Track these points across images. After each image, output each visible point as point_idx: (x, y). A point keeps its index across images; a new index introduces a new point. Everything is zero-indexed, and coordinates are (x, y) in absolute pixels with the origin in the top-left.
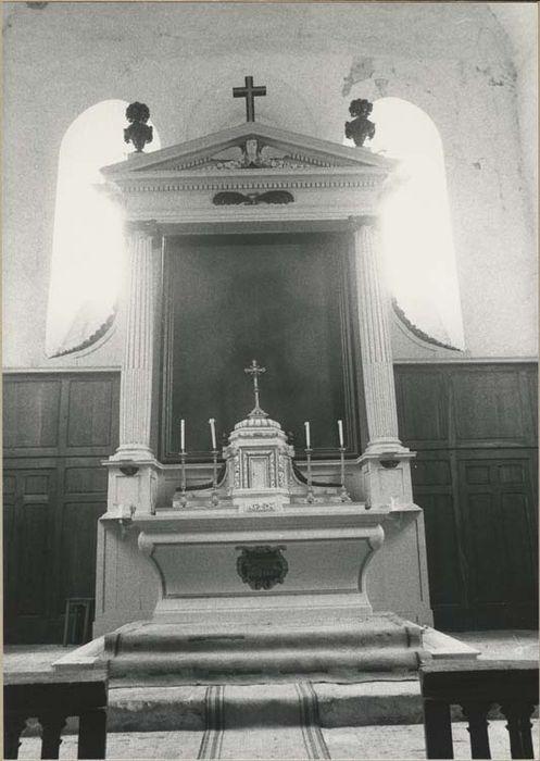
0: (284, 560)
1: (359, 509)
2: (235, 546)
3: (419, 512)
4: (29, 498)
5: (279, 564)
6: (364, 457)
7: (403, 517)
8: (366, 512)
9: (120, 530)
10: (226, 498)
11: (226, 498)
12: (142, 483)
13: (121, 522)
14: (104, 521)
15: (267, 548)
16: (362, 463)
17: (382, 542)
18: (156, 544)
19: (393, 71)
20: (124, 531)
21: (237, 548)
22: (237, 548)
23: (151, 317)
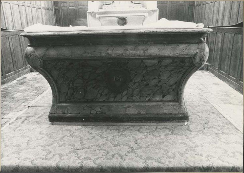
0: (127, 20)
1: (144, 9)
2: (116, 17)
3: (157, 10)
4: (70, 8)
5: (126, 21)
6: (98, 165)
7: (154, 11)
8: (146, 10)
9: (92, 14)
10: (114, 7)
11: (114, 7)
12: (199, 45)
13: (92, 12)
14: (88, 12)
15: (123, 17)
16: (98, 164)
17: (148, 16)
18: (100, 17)
19: (135, 161)
20: (93, 15)
21: (117, 18)
22: (117, 18)
23: (146, 31)
